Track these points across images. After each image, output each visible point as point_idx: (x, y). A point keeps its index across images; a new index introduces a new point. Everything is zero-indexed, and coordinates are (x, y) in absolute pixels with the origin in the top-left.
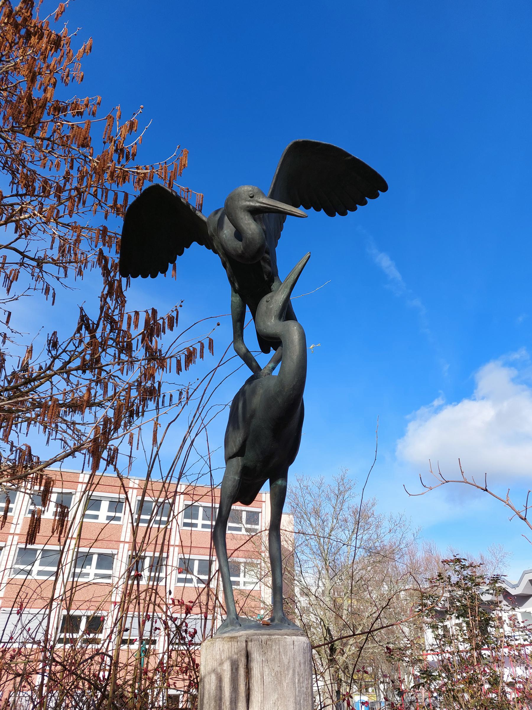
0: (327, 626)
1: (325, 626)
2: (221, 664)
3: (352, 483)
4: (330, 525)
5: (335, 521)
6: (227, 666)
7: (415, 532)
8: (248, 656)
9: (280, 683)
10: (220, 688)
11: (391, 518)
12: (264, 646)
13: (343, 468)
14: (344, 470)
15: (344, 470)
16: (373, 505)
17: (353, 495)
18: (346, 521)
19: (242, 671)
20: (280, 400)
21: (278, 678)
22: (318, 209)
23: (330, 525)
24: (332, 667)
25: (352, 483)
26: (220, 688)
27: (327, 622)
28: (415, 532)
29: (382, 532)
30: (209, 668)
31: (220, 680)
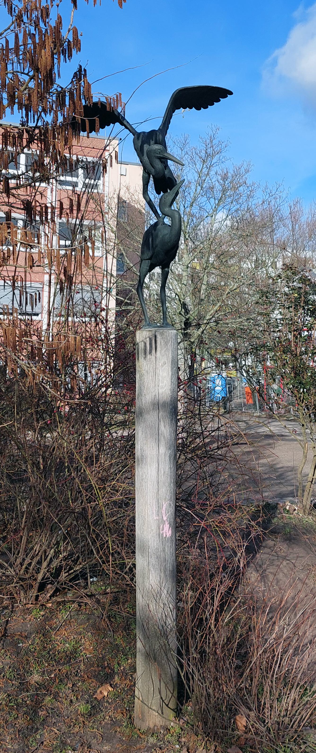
0: (182, 301)
1: (180, 301)
2: (146, 339)
3: (223, 145)
4: (192, 195)
5: (199, 188)
6: (148, 339)
7: (292, 204)
8: (156, 337)
9: (167, 345)
10: (145, 346)
11: (266, 188)
12: (162, 334)
13: (213, 126)
14: (214, 129)
15: (214, 129)
16: (247, 171)
17: (223, 160)
18: (212, 188)
19: (153, 341)
20: (169, 244)
21: (166, 343)
22: (191, 108)
23: (192, 195)
24: (186, 341)
25: (223, 145)
26: (145, 346)
27: (182, 297)
28: (292, 204)
29: (253, 203)
30: (141, 340)
31: (145, 344)
